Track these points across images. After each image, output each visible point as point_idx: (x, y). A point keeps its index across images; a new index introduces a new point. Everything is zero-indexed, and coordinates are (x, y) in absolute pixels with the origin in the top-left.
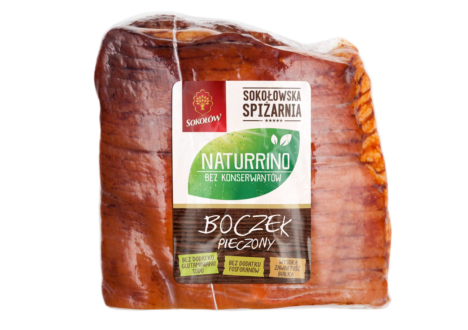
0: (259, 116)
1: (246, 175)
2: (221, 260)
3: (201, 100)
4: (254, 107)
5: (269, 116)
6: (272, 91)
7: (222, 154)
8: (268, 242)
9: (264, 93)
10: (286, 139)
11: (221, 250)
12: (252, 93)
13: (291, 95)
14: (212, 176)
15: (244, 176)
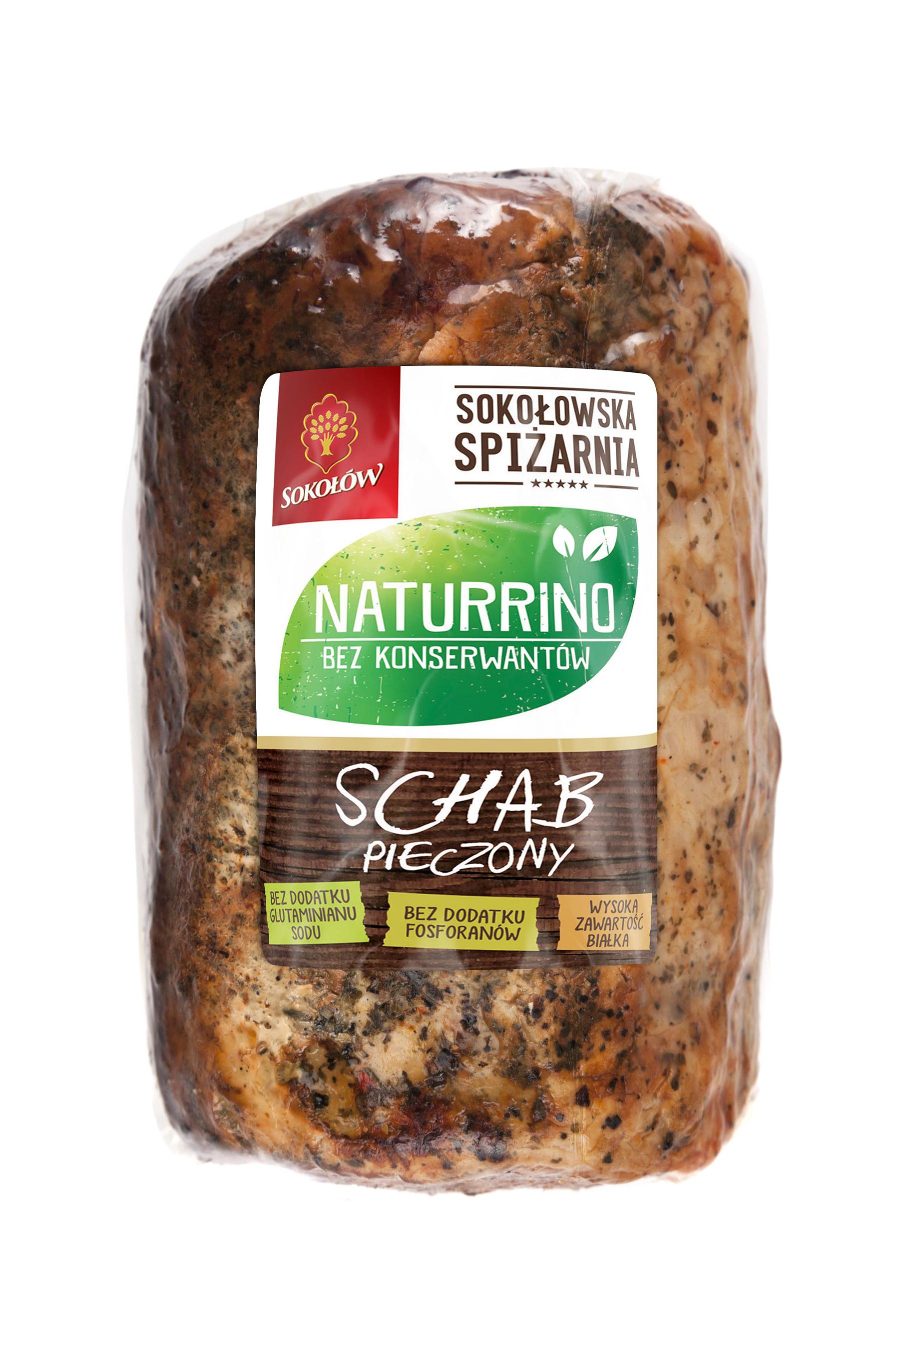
0: (511, 469)
1: (464, 649)
2: (377, 907)
3: (323, 424)
4: (492, 443)
5: (543, 469)
6: (550, 398)
7: (379, 585)
8: (549, 851)
9: (525, 402)
10: (601, 542)
11: (376, 876)
12: (485, 402)
13: (609, 410)
14: (343, 652)
15: (457, 653)
